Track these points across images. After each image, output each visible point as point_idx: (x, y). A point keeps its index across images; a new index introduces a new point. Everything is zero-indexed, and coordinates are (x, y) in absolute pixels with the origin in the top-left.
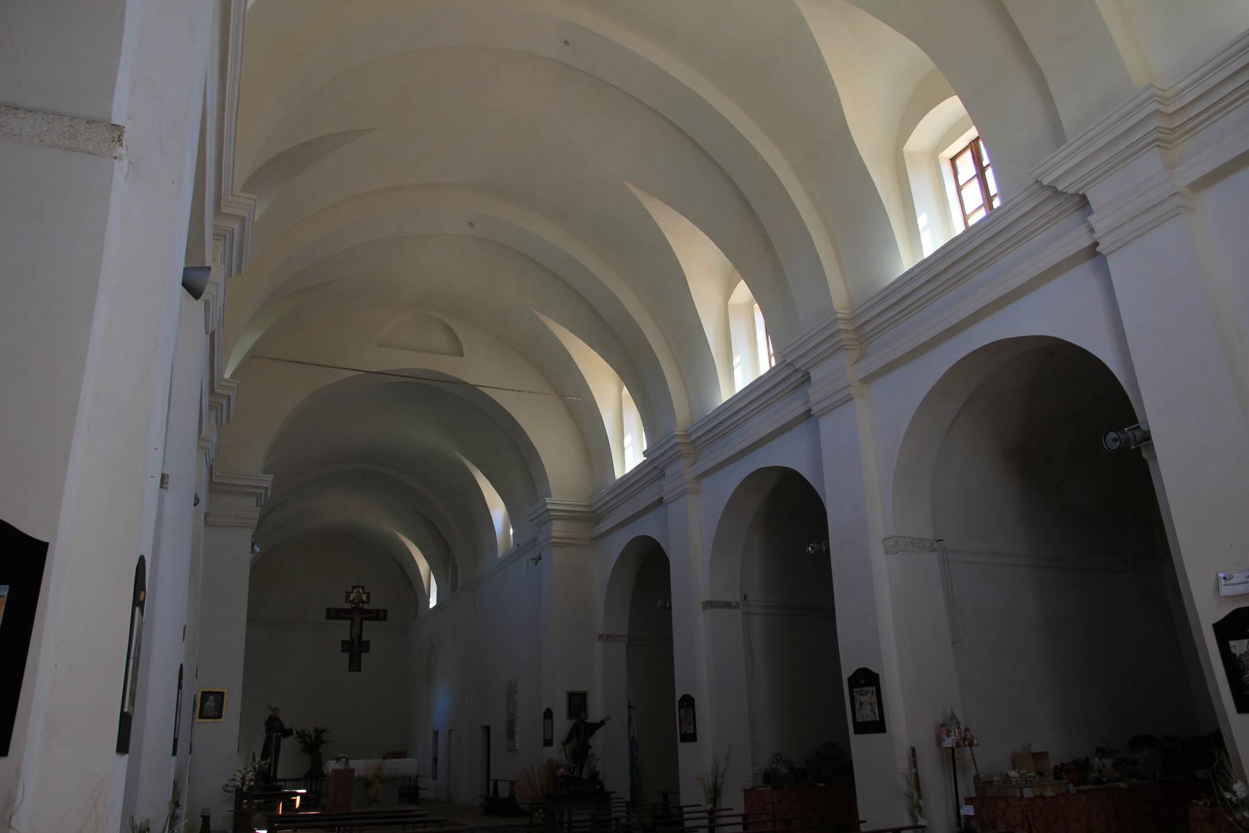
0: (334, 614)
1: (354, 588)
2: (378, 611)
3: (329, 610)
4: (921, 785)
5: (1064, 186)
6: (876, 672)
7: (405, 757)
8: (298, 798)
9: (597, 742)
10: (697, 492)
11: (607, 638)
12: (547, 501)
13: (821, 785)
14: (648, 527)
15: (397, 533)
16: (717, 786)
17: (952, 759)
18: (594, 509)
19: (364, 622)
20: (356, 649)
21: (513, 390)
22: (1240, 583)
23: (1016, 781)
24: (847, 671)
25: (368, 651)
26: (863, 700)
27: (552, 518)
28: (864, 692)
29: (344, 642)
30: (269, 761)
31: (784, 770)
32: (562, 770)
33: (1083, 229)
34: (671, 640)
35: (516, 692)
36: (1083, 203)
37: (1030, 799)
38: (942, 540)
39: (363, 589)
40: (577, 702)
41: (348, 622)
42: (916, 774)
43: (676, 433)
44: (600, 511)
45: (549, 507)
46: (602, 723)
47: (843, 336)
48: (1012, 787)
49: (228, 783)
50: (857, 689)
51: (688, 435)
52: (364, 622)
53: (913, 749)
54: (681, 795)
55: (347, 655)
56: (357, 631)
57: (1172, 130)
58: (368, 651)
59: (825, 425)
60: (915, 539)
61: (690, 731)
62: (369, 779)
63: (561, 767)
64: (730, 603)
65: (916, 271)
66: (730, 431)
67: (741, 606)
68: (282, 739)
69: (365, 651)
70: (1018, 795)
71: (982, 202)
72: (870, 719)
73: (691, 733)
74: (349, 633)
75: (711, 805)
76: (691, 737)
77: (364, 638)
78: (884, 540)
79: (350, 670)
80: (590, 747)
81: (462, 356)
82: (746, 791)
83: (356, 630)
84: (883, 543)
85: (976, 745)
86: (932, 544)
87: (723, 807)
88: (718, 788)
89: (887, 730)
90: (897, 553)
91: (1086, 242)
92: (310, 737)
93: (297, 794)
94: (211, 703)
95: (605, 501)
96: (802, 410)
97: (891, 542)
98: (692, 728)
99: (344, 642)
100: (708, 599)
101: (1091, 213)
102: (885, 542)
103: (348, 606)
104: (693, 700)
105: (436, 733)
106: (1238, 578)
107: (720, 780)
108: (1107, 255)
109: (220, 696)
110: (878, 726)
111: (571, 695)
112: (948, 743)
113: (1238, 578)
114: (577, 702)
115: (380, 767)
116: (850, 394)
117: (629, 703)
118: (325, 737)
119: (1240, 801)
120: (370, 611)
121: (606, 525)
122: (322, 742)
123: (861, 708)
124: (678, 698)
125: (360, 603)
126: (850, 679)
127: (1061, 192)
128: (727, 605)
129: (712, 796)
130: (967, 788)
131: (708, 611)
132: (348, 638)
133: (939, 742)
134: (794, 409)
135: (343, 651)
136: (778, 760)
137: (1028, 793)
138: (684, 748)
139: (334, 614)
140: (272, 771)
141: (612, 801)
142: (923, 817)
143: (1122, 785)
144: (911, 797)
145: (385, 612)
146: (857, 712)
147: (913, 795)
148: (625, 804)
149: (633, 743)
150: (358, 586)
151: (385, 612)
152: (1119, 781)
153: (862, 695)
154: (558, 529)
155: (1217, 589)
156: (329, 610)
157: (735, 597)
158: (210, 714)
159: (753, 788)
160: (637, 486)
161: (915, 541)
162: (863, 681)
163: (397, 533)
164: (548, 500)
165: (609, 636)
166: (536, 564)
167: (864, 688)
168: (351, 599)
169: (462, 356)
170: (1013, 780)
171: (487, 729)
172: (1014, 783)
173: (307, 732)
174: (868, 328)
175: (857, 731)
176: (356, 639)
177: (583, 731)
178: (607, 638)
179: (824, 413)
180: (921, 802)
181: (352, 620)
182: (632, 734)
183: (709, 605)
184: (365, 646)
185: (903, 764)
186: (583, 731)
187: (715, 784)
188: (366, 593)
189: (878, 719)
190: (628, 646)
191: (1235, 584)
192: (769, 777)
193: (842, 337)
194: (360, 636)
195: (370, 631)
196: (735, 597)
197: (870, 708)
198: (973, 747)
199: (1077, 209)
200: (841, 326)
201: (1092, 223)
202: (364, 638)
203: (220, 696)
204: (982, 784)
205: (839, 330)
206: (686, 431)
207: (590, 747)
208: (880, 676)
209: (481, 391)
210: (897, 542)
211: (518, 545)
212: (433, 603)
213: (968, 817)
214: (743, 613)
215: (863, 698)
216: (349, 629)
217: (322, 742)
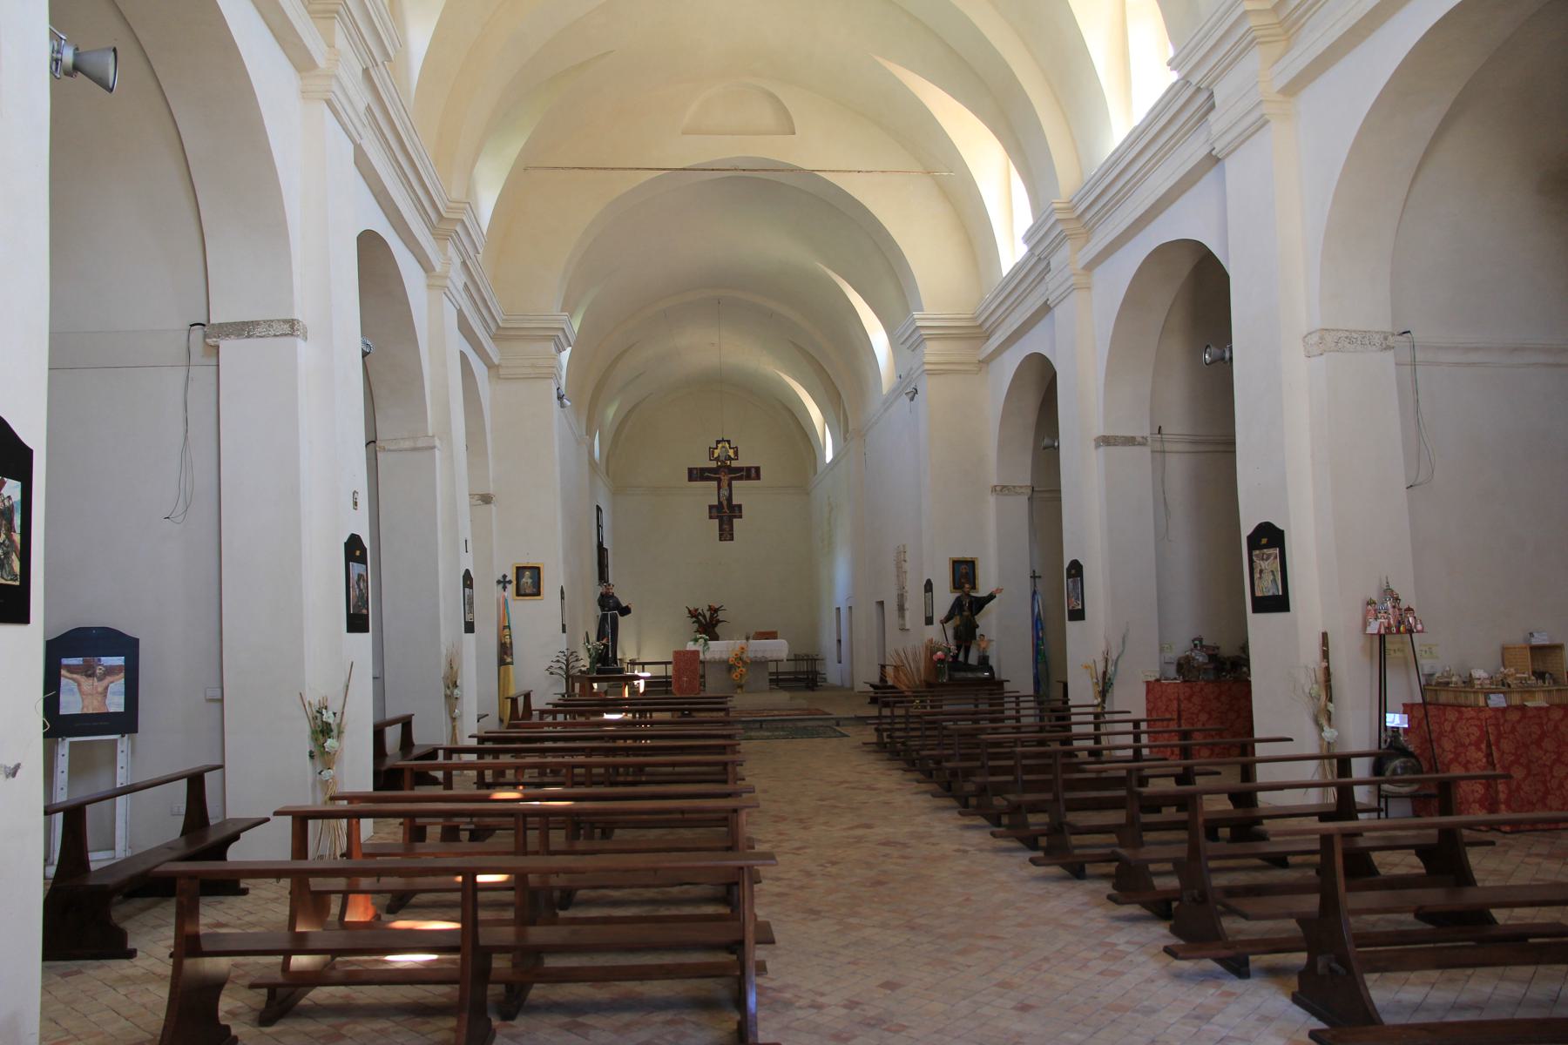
0: (696, 475)
1: (718, 442)
2: (749, 469)
3: (690, 471)
4: (1333, 682)
6: (1281, 528)
7: (775, 638)
8: (642, 683)
9: (989, 622)
10: (1089, 288)
11: (1002, 490)
12: (915, 316)
14: (1035, 343)
15: (782, 374)
16: (1108, 676)
18: (980, 322)
19: (734, 483)
20: (726, 515)
21: (859, 172)
23: (1481, 684)
24: (1247, 528)
25: (741, 517)
26: (1263, 567)
27: (925, 339)
29: (711, 507)
30: (604, 641)
31: (1201, 658)
32: (939, 653)
35: (905, 561)
37: (1496, 710)
38: (1409, 332)
39: (729, 444)
40: (964, 572)
41: (715, 483)
42: (1327, 669)
43: (1056, 206)
45: (919, 324)
46: (991, 597)
47: (1252, 22)
48: (1474, 692)
49: (553, 664)
50: (1257, 552)
51: (1073, 208)
52: (734, 483)
53: (1325, 635)
55: (716, 521)
56: (726, 493)
58: (741, 517)
60: (1355, 331)
62: (731, 663)
63: (939, 650)
68: (619, 618)
69: (736, 517)
70: (1482, 703)
72: (1270, 594)
73: (1079, 610)
74: (716, 498)
75: (1099, 700)
76: (1078, 615)
77: (735, 502)
79: (720, 540)
80: (978, 626)
81: (794, 133)
82: (1148, 683)
83: (725, 492)
84: (1304, 341)
85: (1422, 631)
88: (1109, 679)
89: (1291, 609)
90: (1321, 354)
92: (704, 616)
93: (638, 678)
94: (527, 579)
95: (990, 310)
96: (1204, 151)
97: (1315, 338)
99: (711, 507)
100: (1102, 433)
103: (713, 464)
104: (1081, 567)
105: (838, 609)
107: (1111, 669)
109: (536, 571)
110: (1278, 603)
111: (956, 563)
112: (1374, 628)
114: (964, 572)
115: (743, 648)
118: (721, 615)
120: (740, 469)
122: (719, 621)
123: (1260, 578)
124: (1066, 565)
125: (726, 459)
126: (1250, 538)
128: (1130, 441)
130: (1403, 688)
132: (716, 503)
133: (1365, 624)
135: (711, 517)
136: (1195, 646)
137: (1497, 701)
138: (1072, 627)
139: (696, 475)
140: (610, 652)
141: (1006, 695)
145: (758, 469)
146: (1256, 582)
147: (1320, 696)
150: (723, 440)
151: (758, 469)
153: (1263, 559)
154: (933, 352)
156: (690, 471)
157: (1142, 429)
158: (528, 591)
159: (1158, 680)
162: (1264, 541)
163: (782, 374)
164: (916, 315)
165: (1003, 487)
166: (912, 399)
167: (1265, 550)
168: (716, 455)
169: (794, 133)
170: (1477, 682)
171: (881, 603)
173: (700, 611)
175: (1256, 610)
176: (725, 503)
177: (968, 607)
178: (1002, 490)
180: (1331, 707)
181: (719, 480)
182: (1036, 610)
183: (1106, 441)
184: (736, 511)
185: (1310, 654)
186: (968, 607)
187: (1105, 673)
188: (733, 448)
189: (1280, 593)
192: (1184, 666)
193: (1252, 25)
194: (730, 499)
195: (742, 492)
196: (1142, 429)
197: (1272, 577)
198: (1413, 635)
202: (735, 502)
203: (536, 571)
204: (1431, 686)
205: (1245, 14)
207: (978, 626)
208: (1285, 532)
209: (827, 182)
210: (1322, 338)
211: (900, 377)
212: (829, 456)
213: (1395, 730)
214: (1153, 452)
215: (1264, 565)
216: (716, 492)
217: (719, 621)
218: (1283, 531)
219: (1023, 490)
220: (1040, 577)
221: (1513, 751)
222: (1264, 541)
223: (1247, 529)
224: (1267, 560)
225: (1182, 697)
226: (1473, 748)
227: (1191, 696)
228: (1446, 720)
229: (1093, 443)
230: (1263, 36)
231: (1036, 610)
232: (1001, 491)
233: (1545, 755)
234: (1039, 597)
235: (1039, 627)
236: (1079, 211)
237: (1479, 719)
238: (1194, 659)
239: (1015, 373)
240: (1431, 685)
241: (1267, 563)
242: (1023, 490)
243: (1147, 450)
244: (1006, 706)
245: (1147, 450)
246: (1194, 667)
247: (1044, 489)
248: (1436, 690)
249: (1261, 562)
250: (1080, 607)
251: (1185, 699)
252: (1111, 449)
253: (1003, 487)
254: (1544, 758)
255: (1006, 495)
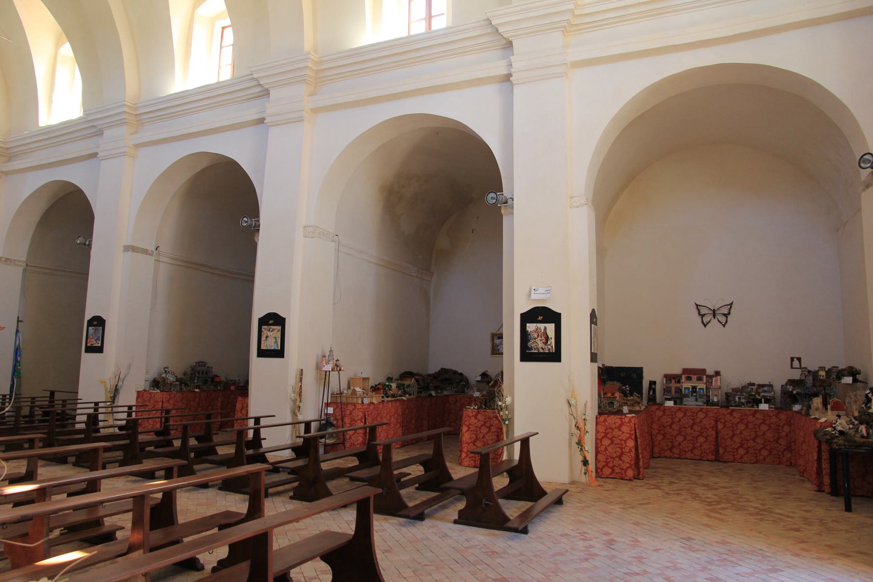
5: (503, 30)
6: (105, 319)
13: (197, 390)
14: (75, 176)
16: (117, 388)
17: (324, 378)
22: (541, 294)
24: (258, 312)
28: (271, 330)
31: (171, 378)
33: (504, 63)
34: (88, 274)
36: (509, 45)
42: (301, 386)
44: (13, 150)
47: (308, 72)
50: (266, 327)
51: (137, 109)
54: (79, 394)
57: (571, 25)
59: (274, 134)
61: (97, 345)
64: (147, 250)
65: (382, 46)
66: (190, 113)
67: (154, 255)
71: (424, 17)
72: (272, 348)
78: (305, 227)
82: (138, 392)
86: (333, 236)
87: (120, 405)
88: (118, 390)
90: (313, 237)
91: (504, 71)
98: (100, 342)
101: (513, 55)
102: (306, 229)
106: (541, 290)
107: (120, 383)
108: (515, 84)
113: (541, 290)
116: (302, 117)
117: (18, 317)
119: (800, 401)
121: (18, 164)
123: (266, 340)
126: (88, 321)
127: (500, 34)
128: (145, 252)
129: (112, 395)
131: (130, 253)
134: (250, 113)
138: (88, 360)
142: (300, 414)
143: (403, 398)
144: (294, 401)
148: (30, 399)
149: (17, 350)
152: (401, 396)
153: (269, 331)
155: (530, 295)
160: (66, 137)
161: (325, 232)
167: (272, 327)
172: (358, 395)
174: (327, 73)
175: (86, 351)
179: (276, 124)
180: (301, 405)
182: (17, 343)
183: (127, 248)
185: (292, 379)
189: (279, 349)
190: (25, 270)
191: (539, 294)
199: (500, 49)
200: (310, 65)
201: (512, 61)
205: (307, 67)
206: (134, 104)
210: (315, 230)
218: (105, 320)
219: (21, 263)
220: (22, 321)
221: (786, 444)
222: (540, 318)
223: (88, 317)
224: (272, 331)
225: (164, 400)
226: (729, 440)
227: (169, 400)
228: (347, 410)
229: (122, 249)
230: (309, 81)
231: (17, 343)
232: (5, 261)
233: (622, 434)
234: (20, 334)
235: (18, 354)
236: (140, 112)
237: (363, 409)
238: (167, 379)
239: (164, 171)
240: (334, 394)
241: (272, 333)
242: (21, 263)
243: (152, 258)
244: (78, 411)
245: (152, 258)
246: (168, 383)
247: (32, 265)
248: (337, 397)
249: (268, 332)
250: (100, 345)
251: (166, 401)
252: (135, 254)
253: (7, 259)
254: (622, 436)
255: (9, 265)
